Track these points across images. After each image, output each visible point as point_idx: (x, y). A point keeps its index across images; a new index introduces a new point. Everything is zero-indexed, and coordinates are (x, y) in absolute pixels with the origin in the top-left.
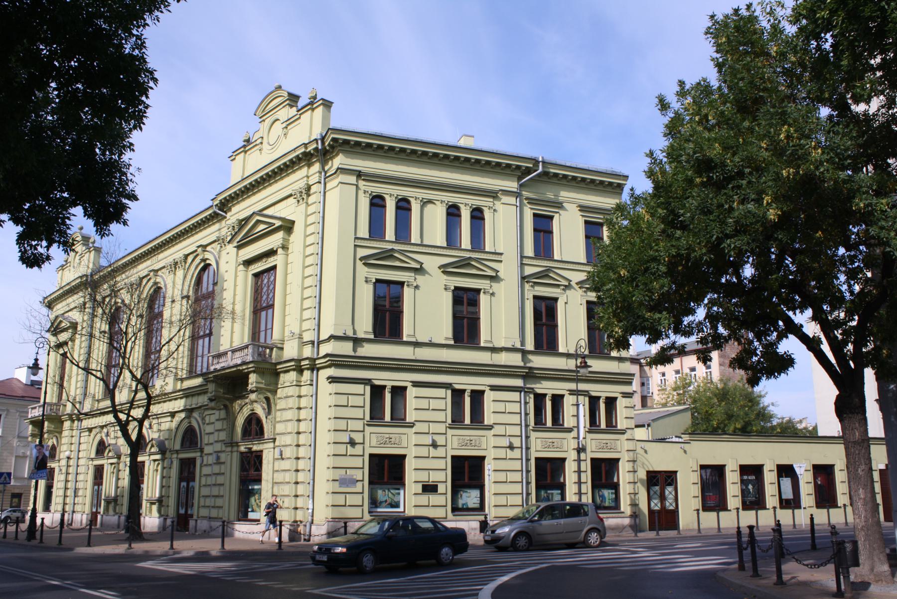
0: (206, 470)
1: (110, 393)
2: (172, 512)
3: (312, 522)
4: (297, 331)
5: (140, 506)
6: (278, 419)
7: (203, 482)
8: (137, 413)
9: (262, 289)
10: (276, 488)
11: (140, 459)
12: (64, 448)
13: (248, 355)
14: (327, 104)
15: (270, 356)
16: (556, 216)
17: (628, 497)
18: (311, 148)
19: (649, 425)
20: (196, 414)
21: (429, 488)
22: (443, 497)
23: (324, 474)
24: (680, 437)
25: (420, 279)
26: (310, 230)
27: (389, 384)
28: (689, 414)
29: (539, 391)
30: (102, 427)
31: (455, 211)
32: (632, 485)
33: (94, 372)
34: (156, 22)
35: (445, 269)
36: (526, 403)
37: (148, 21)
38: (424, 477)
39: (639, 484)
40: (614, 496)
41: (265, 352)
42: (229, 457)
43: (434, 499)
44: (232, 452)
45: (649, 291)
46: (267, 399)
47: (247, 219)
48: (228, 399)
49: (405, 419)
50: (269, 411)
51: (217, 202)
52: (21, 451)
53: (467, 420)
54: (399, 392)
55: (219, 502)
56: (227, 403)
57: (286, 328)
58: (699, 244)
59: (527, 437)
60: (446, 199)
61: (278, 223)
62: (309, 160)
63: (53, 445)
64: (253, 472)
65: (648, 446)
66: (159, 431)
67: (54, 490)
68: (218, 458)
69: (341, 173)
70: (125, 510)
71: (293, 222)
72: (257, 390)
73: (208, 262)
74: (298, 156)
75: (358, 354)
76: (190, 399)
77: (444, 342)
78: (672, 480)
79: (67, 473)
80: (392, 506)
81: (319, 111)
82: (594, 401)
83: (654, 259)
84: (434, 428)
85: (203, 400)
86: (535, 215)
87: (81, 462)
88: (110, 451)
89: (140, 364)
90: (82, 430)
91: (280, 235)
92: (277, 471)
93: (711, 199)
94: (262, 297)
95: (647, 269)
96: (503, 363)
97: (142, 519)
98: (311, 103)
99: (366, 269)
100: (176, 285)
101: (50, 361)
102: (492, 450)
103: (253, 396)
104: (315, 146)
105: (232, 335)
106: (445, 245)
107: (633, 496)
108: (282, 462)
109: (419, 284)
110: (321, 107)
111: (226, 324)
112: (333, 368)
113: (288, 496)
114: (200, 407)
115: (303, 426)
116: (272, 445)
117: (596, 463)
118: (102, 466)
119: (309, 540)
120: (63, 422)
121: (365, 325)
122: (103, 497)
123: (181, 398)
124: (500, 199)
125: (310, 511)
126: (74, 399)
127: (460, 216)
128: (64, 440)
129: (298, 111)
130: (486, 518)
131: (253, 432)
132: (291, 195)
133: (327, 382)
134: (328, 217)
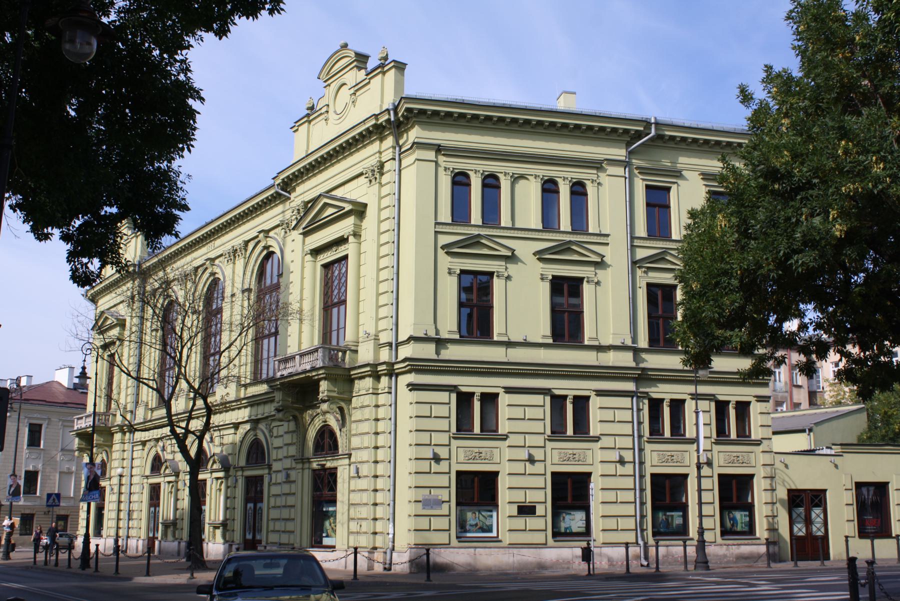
0: (275, 490)
1: (165, 403)
2: (237, 537)
3: (393, 549)
4: (372, 331)
5: (201, 530)
6: (353, 432)
7: (272, 503)
8: (196, 425)
9: (333, 282)
10: (352, 510)
11: (201, 477)
12: (115, 464)
13: (318, 360)
14: (400, 67)
15: (343, 360)
16: (674, 188)
17: (765, 520)
18: (382, 119)
19: (810, 430)
20: (262, 426)
21: (526, 510)
22: (542, 520)
23: (405, 495)
24: (831, 448)
25: (512, 269)
26: (385, 214)
27: (478, 391)
28: (864, 416)
29: (654, 396)
30: (157, 440)
31: (552, 187)
32: (769, 506)
33: (145, 381)
34: (200, 42)
35: (540, 255)
36: (639, 410)
37: (192, 41)
38: (519, 496)
39: (778, 505)
40: (747, 519)
41: (337, 355)
42: (300, 475)
43: (532, 522)
44: (303, 469)
45: (719, 307)
46: (341, 409)
47: (315, 200)
48: (297, 409)
49: (497, 430)
50: (343, 423)
51: (279, 181)
52: (65, 467)
53: (570, 431)
54: (489, 399)
55: (290, 526)
56: (297, 413)
57: (361, 328)
58: (767, 259)
59: (641, 450)
60: (541, 173)
61: (348, 207)
62: (381, 133)
63: (103, 460)
64: (326, 492)
65: (789, 459)
66: (222, 444)
67: (105, 512)
68: (288, 476)
69: (417, 148)
70: (185, 535)
71: (365, 205)
72: (329, 400)
73: (271, 249)
74: (368, 129)
75: (441, 357)
76: (255, 408)
77: (541, 341)
78: (820, 501)
79: (120, 493)
80: (483, 530)
81: (391, 75)
82: (721, 407)
83: (725, 273)
84: (531, 440)
85: (268, 409)
86: (647, 187)
87: (135, 480)
88: (167, 467)
89: (198, 374)
90: (134, 444)
91: (351, 220)
92: (354, 491)
93: (780, 211)
94: (332, 292)
95: (717, 284)
96: (610, 364)
97: (205, 545)
98: (382, 66)
99: (449, 259)
100: (236, 277)
101: (96, 368)
102: (600, 465)
103: (324, 407)
104: (386, 117)
105: (300, 336)
106: (541, 227)
107: (770, 519)
108: (359, 481)
109: (510, 274)
110: (393, 70)
111: (293, 328)
112: (413, 374)
113: (366, 519)
114: (267, 417)
115: (381, 440)
116: (346, 461)
117: (725, 481)
118: (159, 485)
119: (390, 569)
120: (113, 434)
121: (449, 325)
122: (161, 520)
123: (245, 407)
124: (605, 170)
125: (391, 536)
126: (125, 408)
127: (558, 192)
128: (115, 455)
129: (367, 75)
130: (588, 544)
131: (326, 447)
132: (361, 174)
133: (406, 390)
134: (406, 196)
